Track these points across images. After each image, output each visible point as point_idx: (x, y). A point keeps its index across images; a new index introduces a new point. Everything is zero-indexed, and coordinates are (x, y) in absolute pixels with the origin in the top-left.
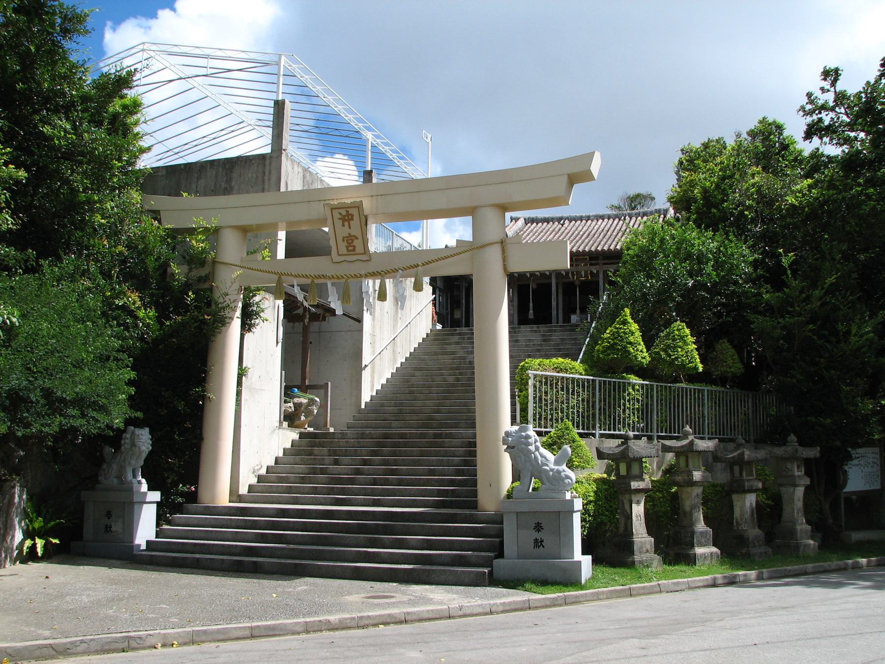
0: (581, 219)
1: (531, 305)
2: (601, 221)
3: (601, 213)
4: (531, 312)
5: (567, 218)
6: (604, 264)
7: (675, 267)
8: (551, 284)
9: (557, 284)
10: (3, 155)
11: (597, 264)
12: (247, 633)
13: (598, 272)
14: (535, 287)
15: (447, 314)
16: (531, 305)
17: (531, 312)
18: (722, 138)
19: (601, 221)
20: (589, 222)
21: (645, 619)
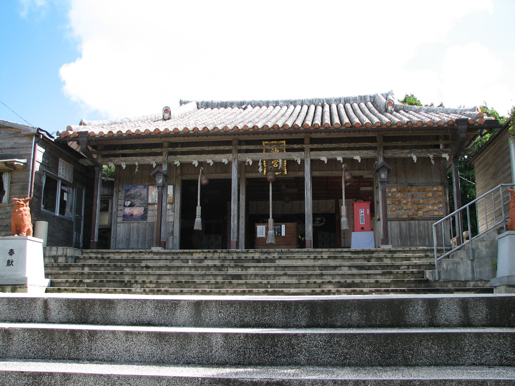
0: (267, 104)
1: (199, 209)
2: (292, 107)
3: (293, 98)
4: (198, 220)
5: (250, 103)
6: (312, 150)
7: (259, 318)
8: (230, 180)
9: (239, 179)
10: (1, 214)
11: (302, 150)
12: (309, 268)
13: (303, 161)
14: (205, 182)
15: (78, 221)
16: (199, 209)
17: (198, 220)
18: (392, 91)
19: (292, 107)
20: (278, 108)
21: (186, 253)
